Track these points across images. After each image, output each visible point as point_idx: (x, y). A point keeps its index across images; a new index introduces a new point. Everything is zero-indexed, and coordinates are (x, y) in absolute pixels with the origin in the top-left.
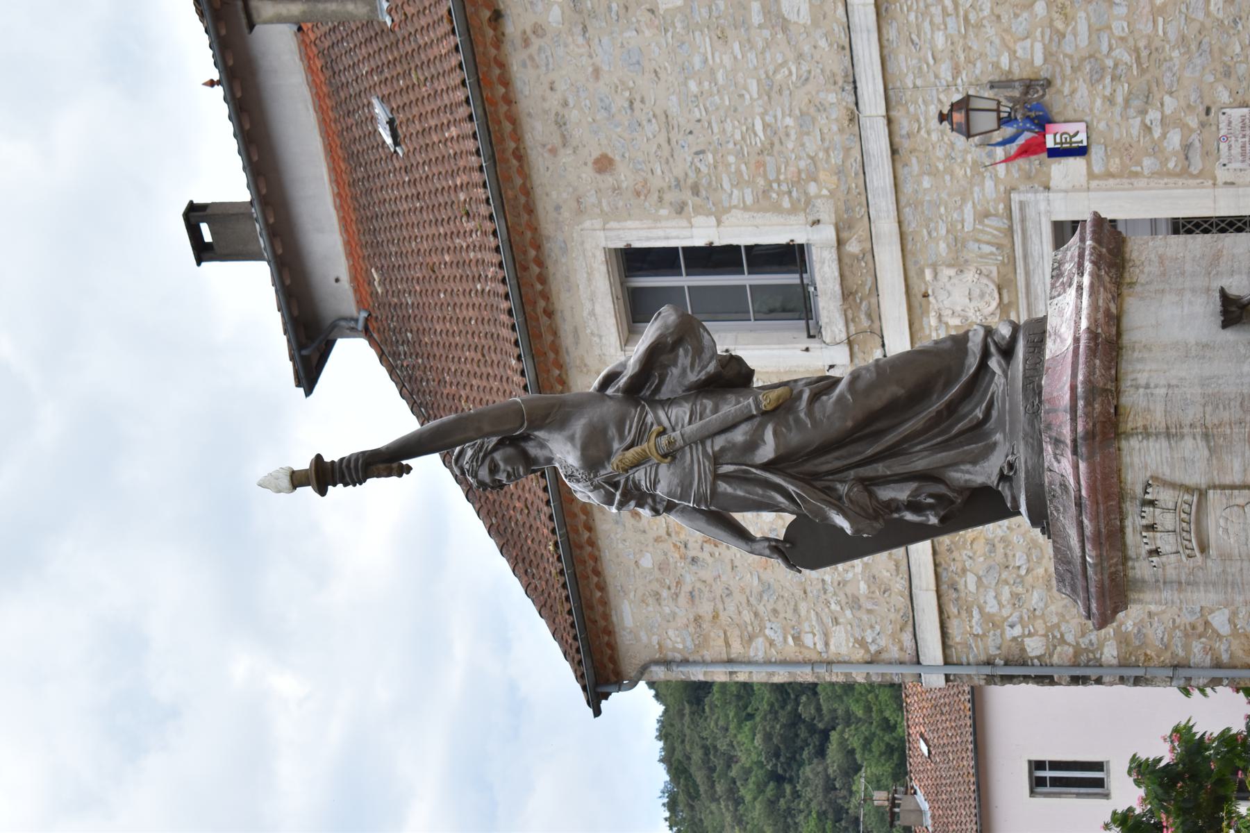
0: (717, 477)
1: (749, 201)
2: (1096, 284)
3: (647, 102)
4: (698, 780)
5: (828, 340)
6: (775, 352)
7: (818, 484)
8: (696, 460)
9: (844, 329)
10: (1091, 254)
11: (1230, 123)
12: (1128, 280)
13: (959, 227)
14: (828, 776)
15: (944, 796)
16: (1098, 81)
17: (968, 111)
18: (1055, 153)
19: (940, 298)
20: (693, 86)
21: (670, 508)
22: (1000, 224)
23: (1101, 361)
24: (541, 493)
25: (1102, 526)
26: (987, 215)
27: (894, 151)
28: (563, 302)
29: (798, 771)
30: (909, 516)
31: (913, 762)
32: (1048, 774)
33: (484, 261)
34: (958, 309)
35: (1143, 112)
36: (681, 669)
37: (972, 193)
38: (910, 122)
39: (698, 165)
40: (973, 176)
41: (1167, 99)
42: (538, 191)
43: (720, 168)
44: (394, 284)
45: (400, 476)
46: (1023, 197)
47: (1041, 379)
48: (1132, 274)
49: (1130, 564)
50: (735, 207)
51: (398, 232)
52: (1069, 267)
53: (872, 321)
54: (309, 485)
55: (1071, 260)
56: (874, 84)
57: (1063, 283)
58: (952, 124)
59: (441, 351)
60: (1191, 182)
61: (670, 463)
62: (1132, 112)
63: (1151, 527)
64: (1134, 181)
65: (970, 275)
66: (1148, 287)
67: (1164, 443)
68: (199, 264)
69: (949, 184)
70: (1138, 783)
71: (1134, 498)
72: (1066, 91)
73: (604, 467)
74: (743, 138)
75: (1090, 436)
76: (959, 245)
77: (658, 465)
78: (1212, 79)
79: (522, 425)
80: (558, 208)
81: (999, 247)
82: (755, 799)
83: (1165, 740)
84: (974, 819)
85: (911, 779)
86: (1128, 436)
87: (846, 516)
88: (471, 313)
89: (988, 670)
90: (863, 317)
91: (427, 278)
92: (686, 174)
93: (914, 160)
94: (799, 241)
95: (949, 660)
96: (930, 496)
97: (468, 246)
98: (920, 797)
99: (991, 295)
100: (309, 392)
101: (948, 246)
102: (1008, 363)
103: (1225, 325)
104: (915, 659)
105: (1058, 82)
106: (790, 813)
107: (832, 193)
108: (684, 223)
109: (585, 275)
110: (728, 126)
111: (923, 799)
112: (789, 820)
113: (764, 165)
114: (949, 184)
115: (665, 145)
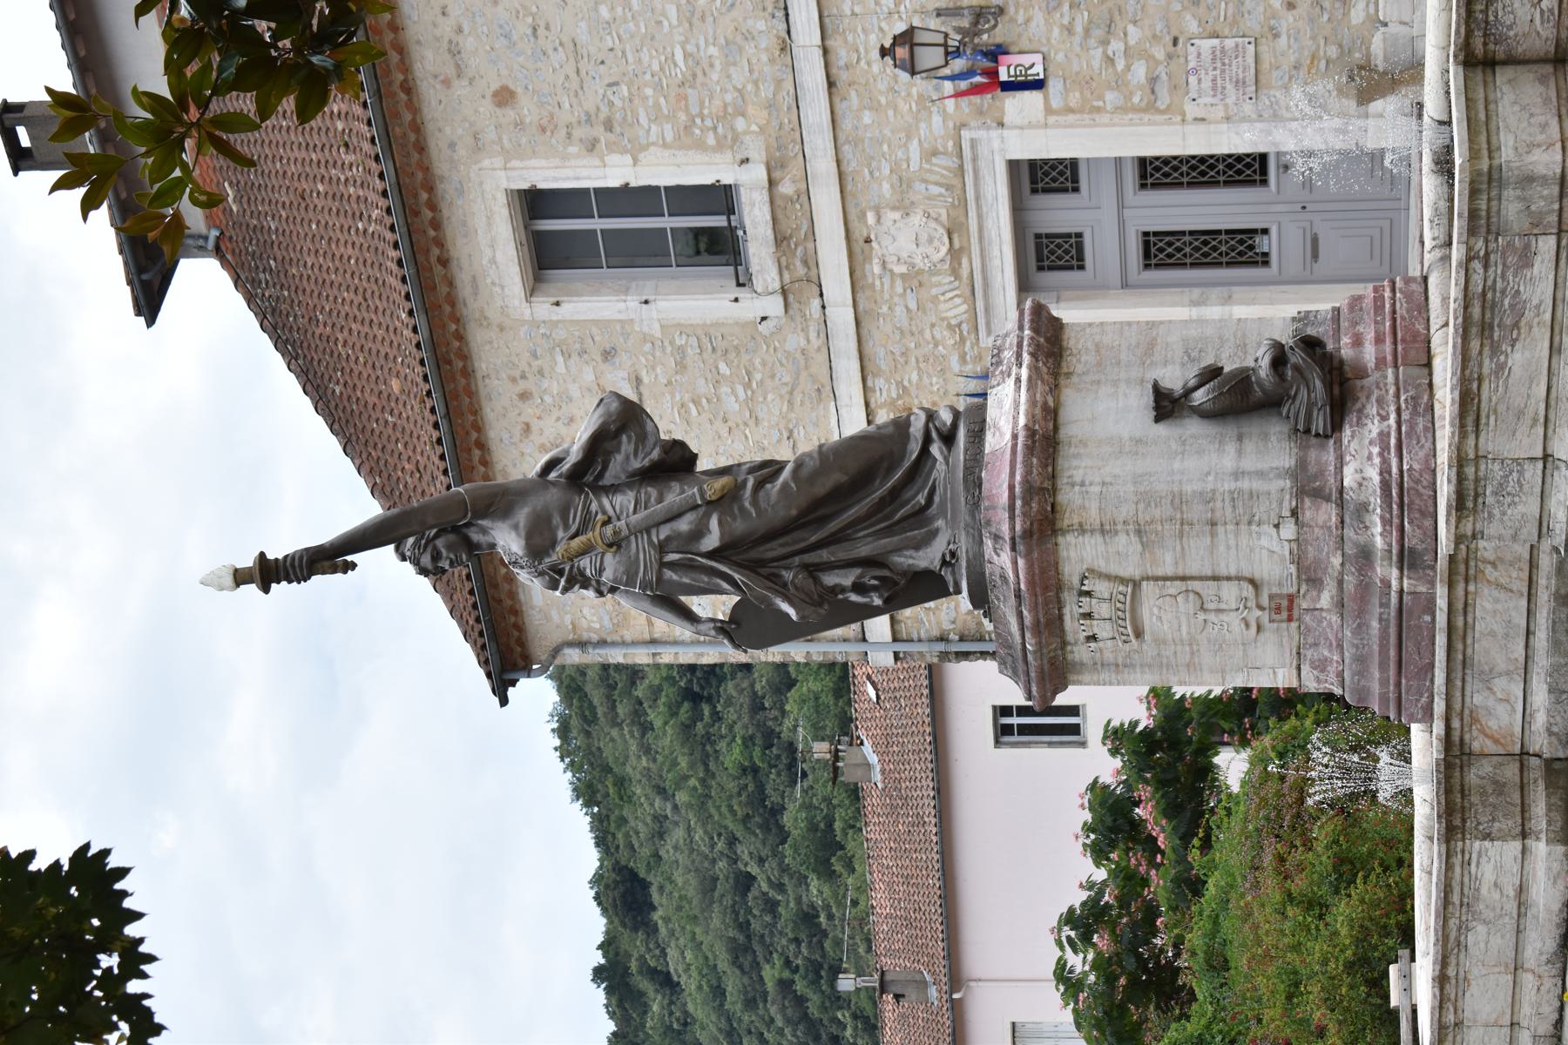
0: (662, 565)
1: (669, 137)
2: (1034, 377)
3: (552, 28)
4: (596, 701)
5: (759, 290)
6: (700, 303)
7: (763, 571)
8: (641, 549)
9: (777, 278)
10: (1029, 345)
11: (1199, 55)
12: (1065, 370)
13: (905, 166)
14: (755, 693)
15: (895, 748)
16: (1055, 9)
17: (912, 45)
18: (1009, 87)
19: (884, 244)
20: (604, 12)
21: (613, 590)
22: (950, 164)
23: (1039, 459)
24: (437, 461)
25: (1041, 616)
26: (935, 153)
27: (831, 84)
28: (460, 249)
29: (718, 687)
30: (854, 597)
31: (860, 709)
32: (1015, 720)
33: (366, 199)
34: (904, 255)
35: (1105, 43)
36: (597, 651)
37: (918, 129)
38: (848, 52)
39: (612, 98)
40: (919, 111)
41: (1131, 29)
42: (430, 127)
43: (636, 101)
44: (253, 204)
45: (345, 572)
46: (974, 134)
47: (981, 471)
48: (1070, 363)
49: (1069, 648)
50: (653, 144)
51: (258, 148)
52: (1008, 355)
53: (809, 268)
54: (252, 582)
55: (1010, 348)
56: (808, 11)
57: (1002, 372)
58: (894, 59)
59: (313, 287)
60: (1159, 118)
61: (616, 552)
62: (1092, 42)
63: (1088, 616)
64: (1097, 117)
65: (917, 219)
66: (1084, 378)
67: (1098, 538)
68: (16, 174)
69: (892, 120)
70: (1114, 752)
71: (1070, 588)
72: (1020, 19)
73: (549, 556)
74: (662, 69)
75: (1028, 534)
76: (904, 186)
77: (603, 554)
78: (1179, 7)
79: (465, 516)
80: (452, 145)
81: (948, 188)
82: (666, 723)
83: (1141, 700)
84: (931, 775)
85: (857, 728)
86: (1064, 532)
87: (792, 604)
88: (350, 251)
89: (941, 647)
90: (798, 263)
91: (296, 204)
92: (598, 109)
93: (853, 94)
94: (726, 180)
95: (899, 636)
96: (875, 578)
97: (347, 180)
98: (868, 749)
99: (940, 239)
100: (151, 322)
101: (892, 186)
102: (949, 450)
103: (1158, 419)
104: (860, 636)
105: (1012, 10)
106: (709, 739)
107: (762, 129)
108: (597, 162)
109: (484, 219)
110: (646, 58)
111: (871, 750)
112: (708, 748)
113: (686, 98)
114: (892, 120)
115: (573, 75)
